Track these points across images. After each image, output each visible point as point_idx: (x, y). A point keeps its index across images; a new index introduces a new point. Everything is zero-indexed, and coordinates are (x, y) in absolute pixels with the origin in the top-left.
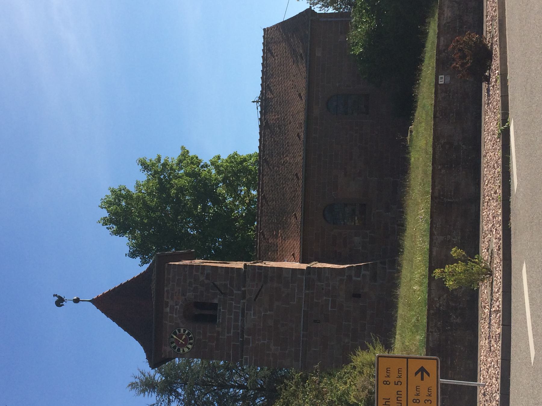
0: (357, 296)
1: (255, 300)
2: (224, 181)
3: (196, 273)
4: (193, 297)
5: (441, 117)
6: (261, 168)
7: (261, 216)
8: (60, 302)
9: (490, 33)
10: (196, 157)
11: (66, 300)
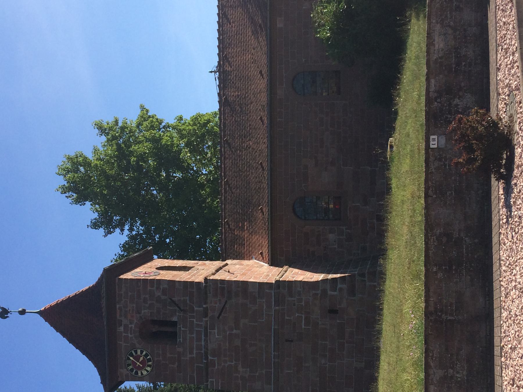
1: (218, 317)
2: (187, 145)
4: (149, 315)
5: (435, 196)
6: (223, 149)
7: (225, 203)
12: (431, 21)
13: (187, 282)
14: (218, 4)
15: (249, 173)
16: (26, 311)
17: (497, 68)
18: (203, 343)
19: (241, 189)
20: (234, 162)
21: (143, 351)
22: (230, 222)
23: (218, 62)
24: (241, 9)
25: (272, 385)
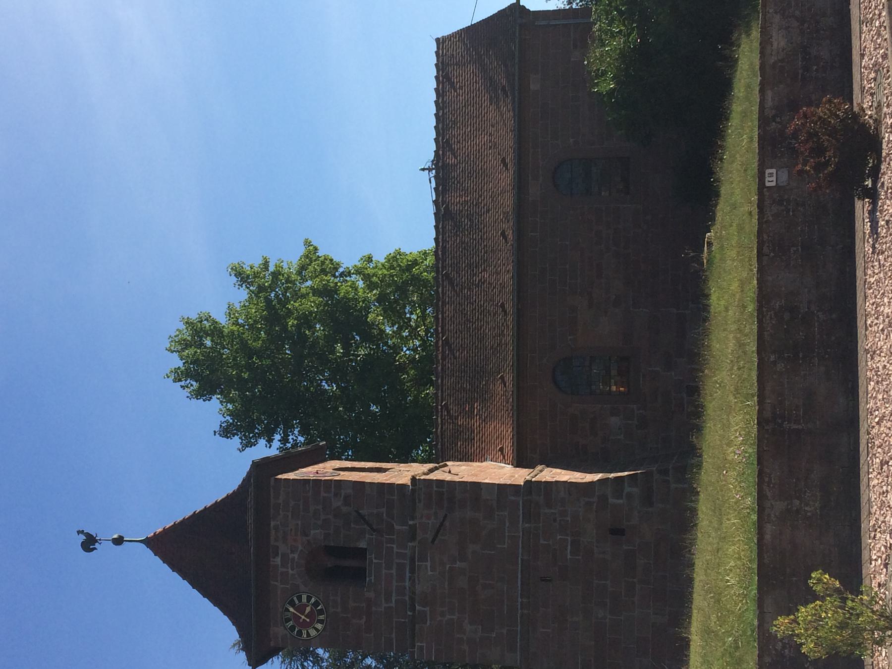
0: (617, 532)
1: (433, 541)
2: (381, 299)
3: (326, 495)
4: (322, 538)
5: (772, 254)
6: (440, 290)
8: (89, 543)
9: (872, 95)
10: (330, 260)
11: (100, 540)
12: (767, 10)
13: (384, 483)
14: (437, 61)
15: (482, 323)
16: (125, 539)
17: (861, 54)
18: (407, 584)
19: (470, 350)
20: (458, 308)
21: (311, 598)
22: (450, 404)
23: (435, 151)
24: (473, 66)
25: (518, 653)
